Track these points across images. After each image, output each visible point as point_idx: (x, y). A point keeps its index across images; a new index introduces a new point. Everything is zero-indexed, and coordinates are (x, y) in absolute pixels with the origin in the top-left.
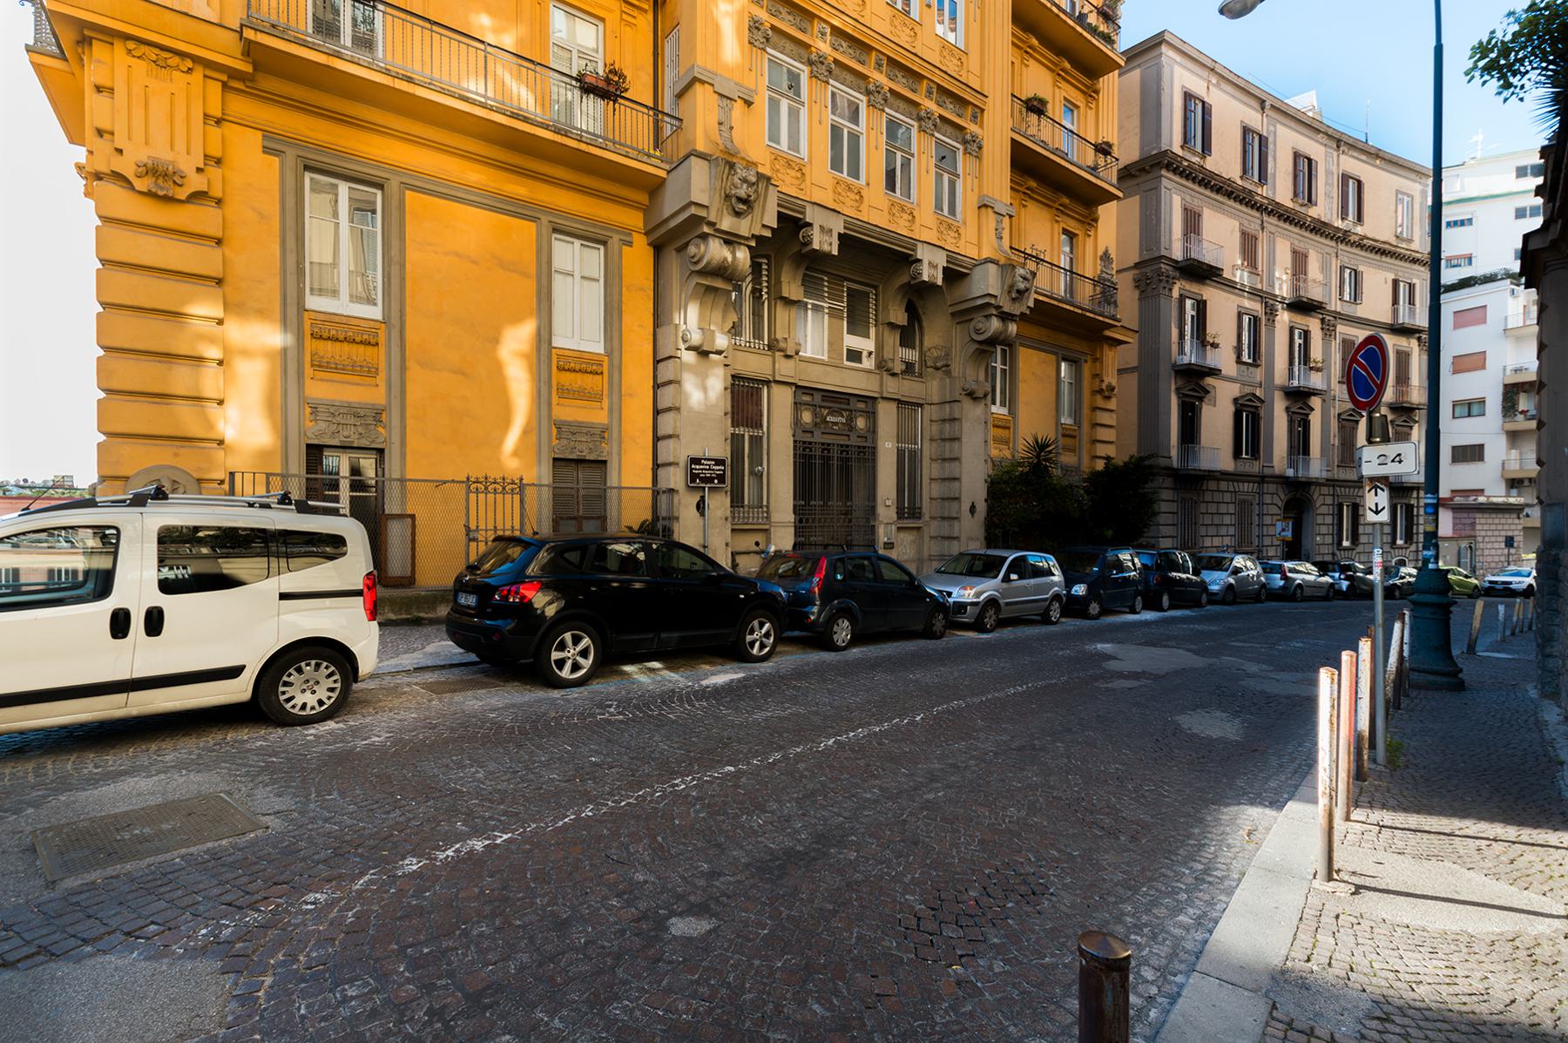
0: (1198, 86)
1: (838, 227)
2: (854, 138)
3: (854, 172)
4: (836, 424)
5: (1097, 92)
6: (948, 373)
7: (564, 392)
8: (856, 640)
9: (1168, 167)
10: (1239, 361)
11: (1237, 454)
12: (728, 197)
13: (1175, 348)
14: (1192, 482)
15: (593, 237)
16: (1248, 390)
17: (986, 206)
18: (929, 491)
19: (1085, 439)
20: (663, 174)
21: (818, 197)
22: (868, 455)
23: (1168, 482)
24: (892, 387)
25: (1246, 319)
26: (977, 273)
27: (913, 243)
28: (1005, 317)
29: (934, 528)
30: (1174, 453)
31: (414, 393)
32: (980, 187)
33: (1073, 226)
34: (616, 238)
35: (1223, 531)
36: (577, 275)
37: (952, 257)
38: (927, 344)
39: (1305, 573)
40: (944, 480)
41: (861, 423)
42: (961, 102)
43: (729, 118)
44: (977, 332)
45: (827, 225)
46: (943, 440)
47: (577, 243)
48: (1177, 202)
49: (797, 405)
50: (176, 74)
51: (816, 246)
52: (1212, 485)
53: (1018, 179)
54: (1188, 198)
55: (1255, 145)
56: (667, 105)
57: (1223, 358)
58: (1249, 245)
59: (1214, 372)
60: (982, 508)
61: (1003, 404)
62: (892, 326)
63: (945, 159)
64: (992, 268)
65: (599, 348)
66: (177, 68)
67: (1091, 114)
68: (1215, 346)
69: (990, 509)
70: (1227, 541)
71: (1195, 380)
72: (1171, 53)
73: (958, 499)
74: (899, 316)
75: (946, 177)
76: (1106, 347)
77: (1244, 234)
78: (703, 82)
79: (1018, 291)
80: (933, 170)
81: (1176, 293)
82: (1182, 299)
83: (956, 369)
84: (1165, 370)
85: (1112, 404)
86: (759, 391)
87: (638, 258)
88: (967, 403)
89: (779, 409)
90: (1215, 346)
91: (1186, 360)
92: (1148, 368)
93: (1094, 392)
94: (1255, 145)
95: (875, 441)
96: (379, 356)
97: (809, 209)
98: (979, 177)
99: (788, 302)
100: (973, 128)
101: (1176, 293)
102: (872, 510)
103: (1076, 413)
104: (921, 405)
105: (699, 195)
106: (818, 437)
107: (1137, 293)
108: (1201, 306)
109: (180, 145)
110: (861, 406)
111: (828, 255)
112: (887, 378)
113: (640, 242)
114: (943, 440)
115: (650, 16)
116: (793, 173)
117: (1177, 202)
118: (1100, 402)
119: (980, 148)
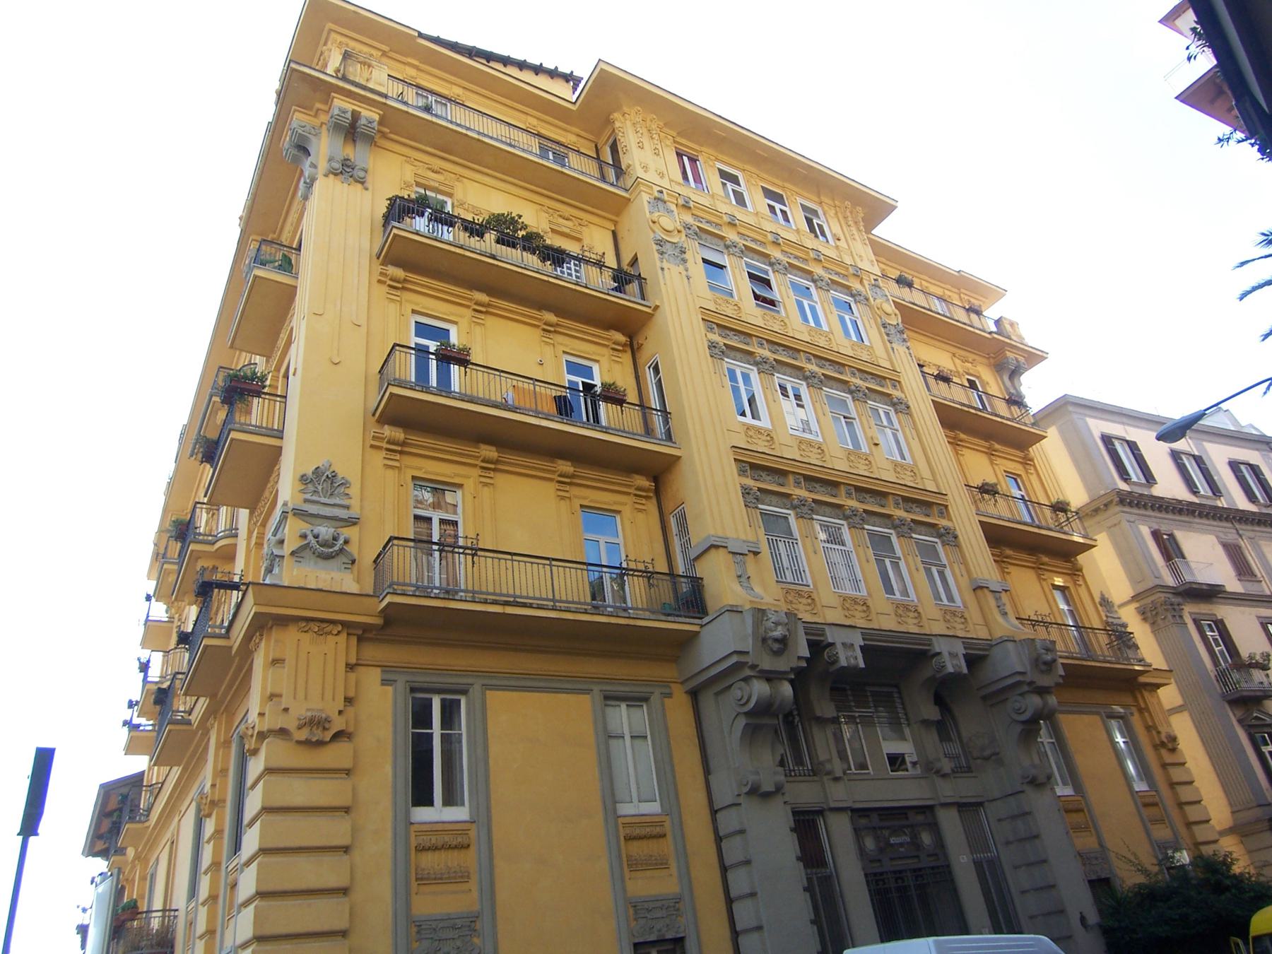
1: (858, 641)
4: (901, 845)
5: (1032, 460)
7: (635, 865)
12: (764, 640)
17: (981, 588)
20: (696, 628)
21: (830, 620)
22: (944, 873)
24: (948, 790)
26: (996, 652)
27: (928, 638)
28: (1042, 691)
32: (968, 571)
34: (657, 692)
36: (627, 738)
38: (964, 734)
40: (1037, 889)
41: (926, 838)
42: (929, 505)
43: (745, 570)
44: (1018, 712)
45: (848, 641)
46: (1020, 840)
47: (623, 706)
49: (857, 831)
50: (329, 637)
51: (843, 663)
53: (997, 551)
54: (1221, 535)
55: (1192, 468)
56: (681, 569)
58: (1235, 555)
61: (1065, 784)
62: (926, 723)
63: (928, 553)
64: (1010, 645)
66: (330, 633)
67: (1034, 478)
73: (1062, 912)
74: (932, 713)
75: (934, 569)
76: (1146, 694)
77: (1226, 546)
78: (717, 547)
79: (1045, 663)
80: (921, 566)
86: (814, 822)
89: (839, 836)
93: (1156, 747)
94: (1192, 468)
95: (946, 856)
96: (469, 859)
97: (828, 630)
99: (821, 721)
100: (943, 522)
104: (981, 804)
108: (1220, 626)
109: (329, 695)
110: (920, 818)
111: (855, 669)
112: (939, 782)
114: (1020, 840)
115: (654, 501)
116: (804, 601)
119: (956, 537)
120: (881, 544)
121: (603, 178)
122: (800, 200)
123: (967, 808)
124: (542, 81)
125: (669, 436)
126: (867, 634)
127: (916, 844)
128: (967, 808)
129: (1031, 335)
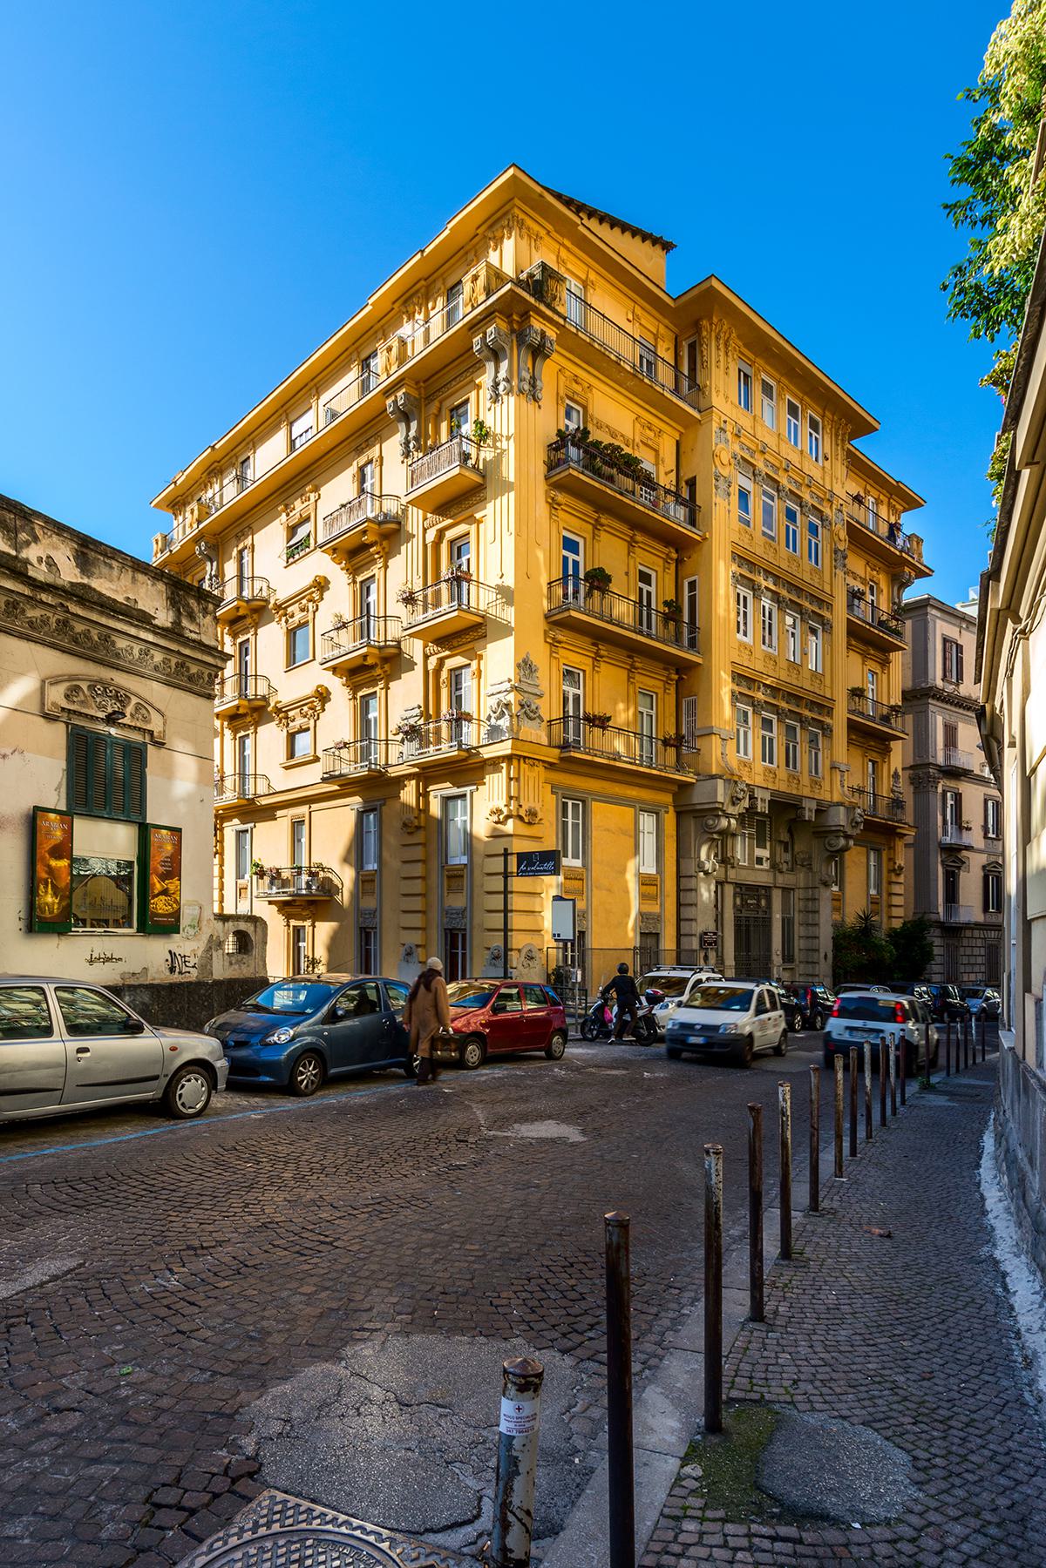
0: (952, 631)
2: (649, 593)
3: (771, 762)
6: (810, 869)
8: (486, 1061)
9: (933, 697)
10: (986, 837)
11: (986, 909)
13: (940, 830)
14: (953, 931)
15: (655, 811)
16: (993, 859)
18: (799, 944)
19: (884, 904)
22: (767, 923)
23: (938, 932)
25: (990, 804)
28: (847, 837)
29: (801, 969)
30: (941, 909)
31: (595, 902)
33: (875, 756)
35: (976, 969)
37: (819, 803)
38: (796, 849)
39: (280, 1496)
41: (763, 903)
42: (821, 706)
48: (940, 720)
49: (735, 895)
52: (968, 933)
57: (975, 838)
59: (969, 848)
60: (830, 955)
63: (813, 741)
65: (653, 871)
68: (969, 829)
69: (835, 957)
70: (980, 977)
71: (954, 855)
72: (934, 612)
74: (785, 837)
81: (940, 790)
82: (944, 793)
83: (815, 867)
84: (933, 847)
85: (901, 879)
87: (670, 819)
88: (822, 889)
90: (969, 829)
91: (948, 840)
92: (921, 849)
93: (889, 871)
98: (831, 749)
100: (828, 720)
101: (940, 790)
102: (768, 958)
103: (878, 886)
105: (720, 799)
106: (744, 914)
107: (912, 789)
108: (958, 797)
113: (671, 809)
117: (940, 720)
118: (894, 879)
120: (791, 730)
121: (676, 390)
122: (764, 376)
123: (786, 890)
124: (603, 231)
125: (693, 644)
126: (774, 793)
127: (758, 905)
128: (786, 890)
129: (928, 557)
